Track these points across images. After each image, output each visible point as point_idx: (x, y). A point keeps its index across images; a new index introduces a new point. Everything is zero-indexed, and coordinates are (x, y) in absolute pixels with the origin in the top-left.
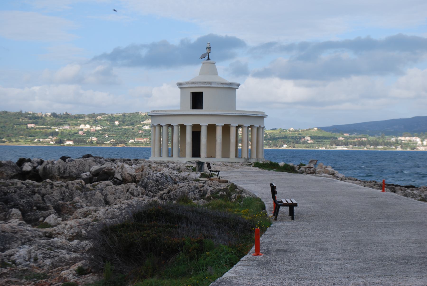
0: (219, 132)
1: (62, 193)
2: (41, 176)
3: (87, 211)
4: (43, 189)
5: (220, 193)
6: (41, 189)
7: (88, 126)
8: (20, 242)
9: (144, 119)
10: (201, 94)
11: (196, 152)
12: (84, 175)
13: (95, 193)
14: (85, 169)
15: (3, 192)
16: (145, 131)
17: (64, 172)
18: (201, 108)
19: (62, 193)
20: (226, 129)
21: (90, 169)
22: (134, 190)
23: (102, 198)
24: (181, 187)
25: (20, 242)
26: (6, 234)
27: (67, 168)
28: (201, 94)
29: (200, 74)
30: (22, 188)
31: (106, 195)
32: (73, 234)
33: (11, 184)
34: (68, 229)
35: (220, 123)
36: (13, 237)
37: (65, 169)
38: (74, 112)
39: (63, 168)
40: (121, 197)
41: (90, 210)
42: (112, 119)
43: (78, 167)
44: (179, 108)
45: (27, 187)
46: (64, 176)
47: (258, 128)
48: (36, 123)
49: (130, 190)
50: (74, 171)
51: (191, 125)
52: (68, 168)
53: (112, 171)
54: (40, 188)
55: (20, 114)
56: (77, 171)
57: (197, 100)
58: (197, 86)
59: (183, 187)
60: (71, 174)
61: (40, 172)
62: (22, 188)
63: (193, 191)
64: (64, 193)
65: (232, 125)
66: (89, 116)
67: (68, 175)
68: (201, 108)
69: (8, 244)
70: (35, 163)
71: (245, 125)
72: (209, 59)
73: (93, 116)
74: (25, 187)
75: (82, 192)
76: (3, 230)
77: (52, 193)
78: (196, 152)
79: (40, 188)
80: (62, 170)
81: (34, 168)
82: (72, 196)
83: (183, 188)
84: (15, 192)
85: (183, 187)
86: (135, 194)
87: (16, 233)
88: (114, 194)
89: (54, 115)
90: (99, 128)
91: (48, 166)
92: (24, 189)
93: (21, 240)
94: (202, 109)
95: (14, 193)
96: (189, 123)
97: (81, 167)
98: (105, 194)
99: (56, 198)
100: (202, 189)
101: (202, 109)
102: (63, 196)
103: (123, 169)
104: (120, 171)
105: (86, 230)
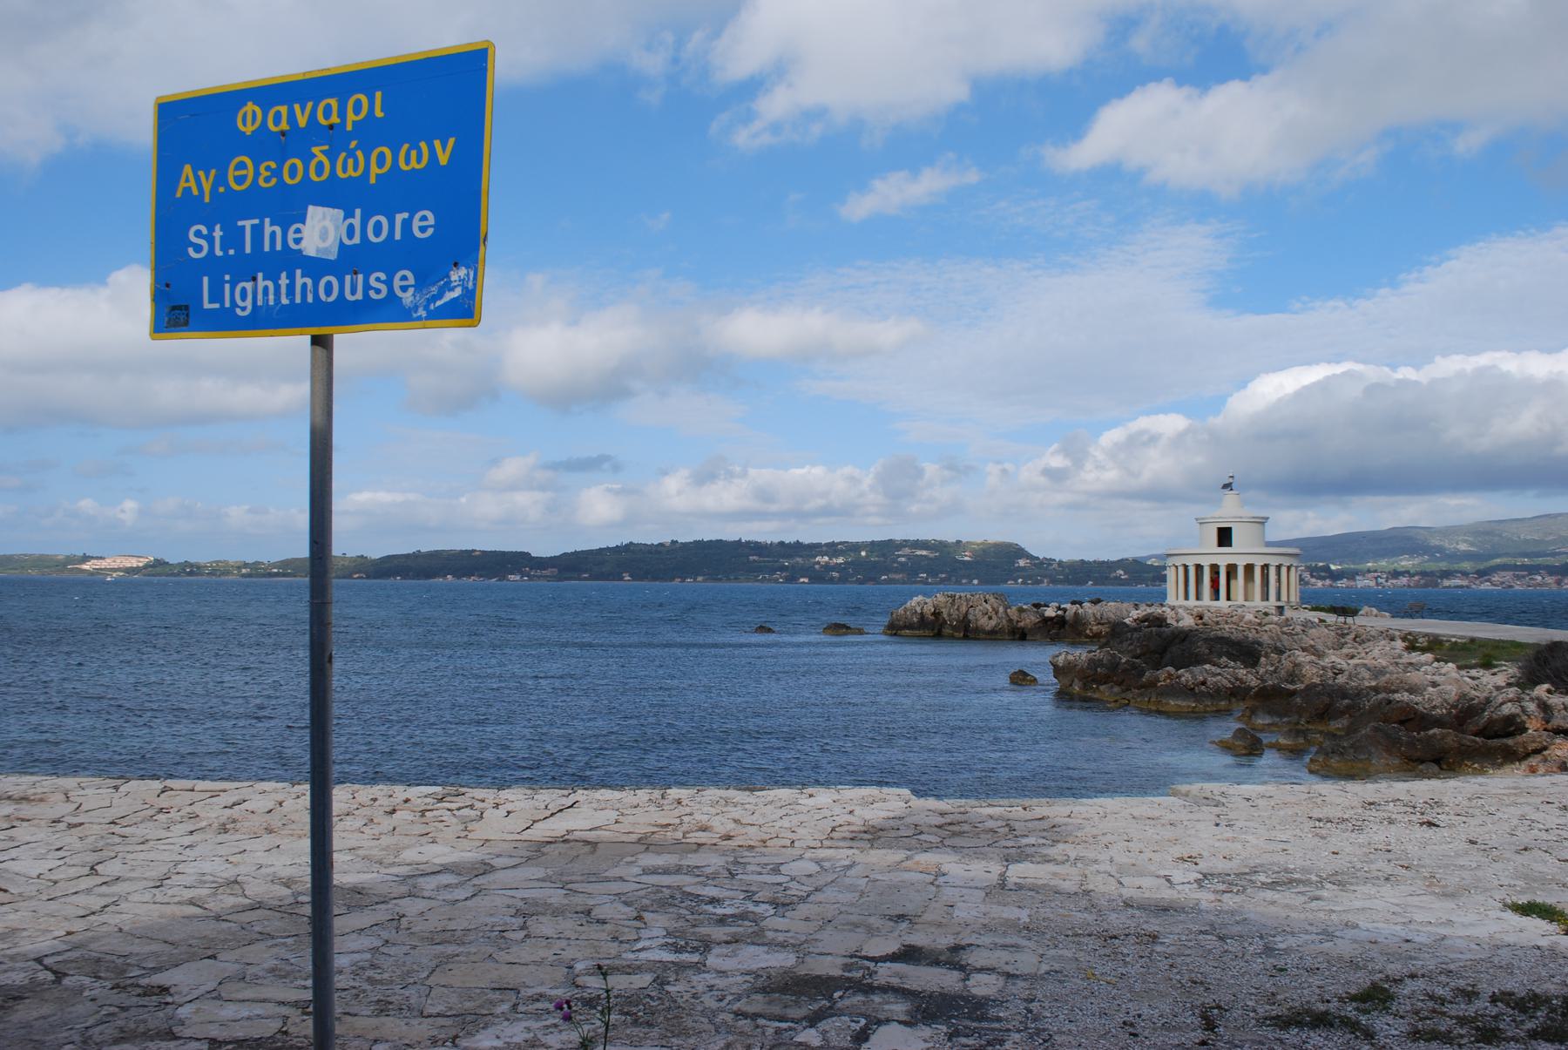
16: (901, 564)
57: (1224, 536)
90: (840, 560)
96: (1223, 563)
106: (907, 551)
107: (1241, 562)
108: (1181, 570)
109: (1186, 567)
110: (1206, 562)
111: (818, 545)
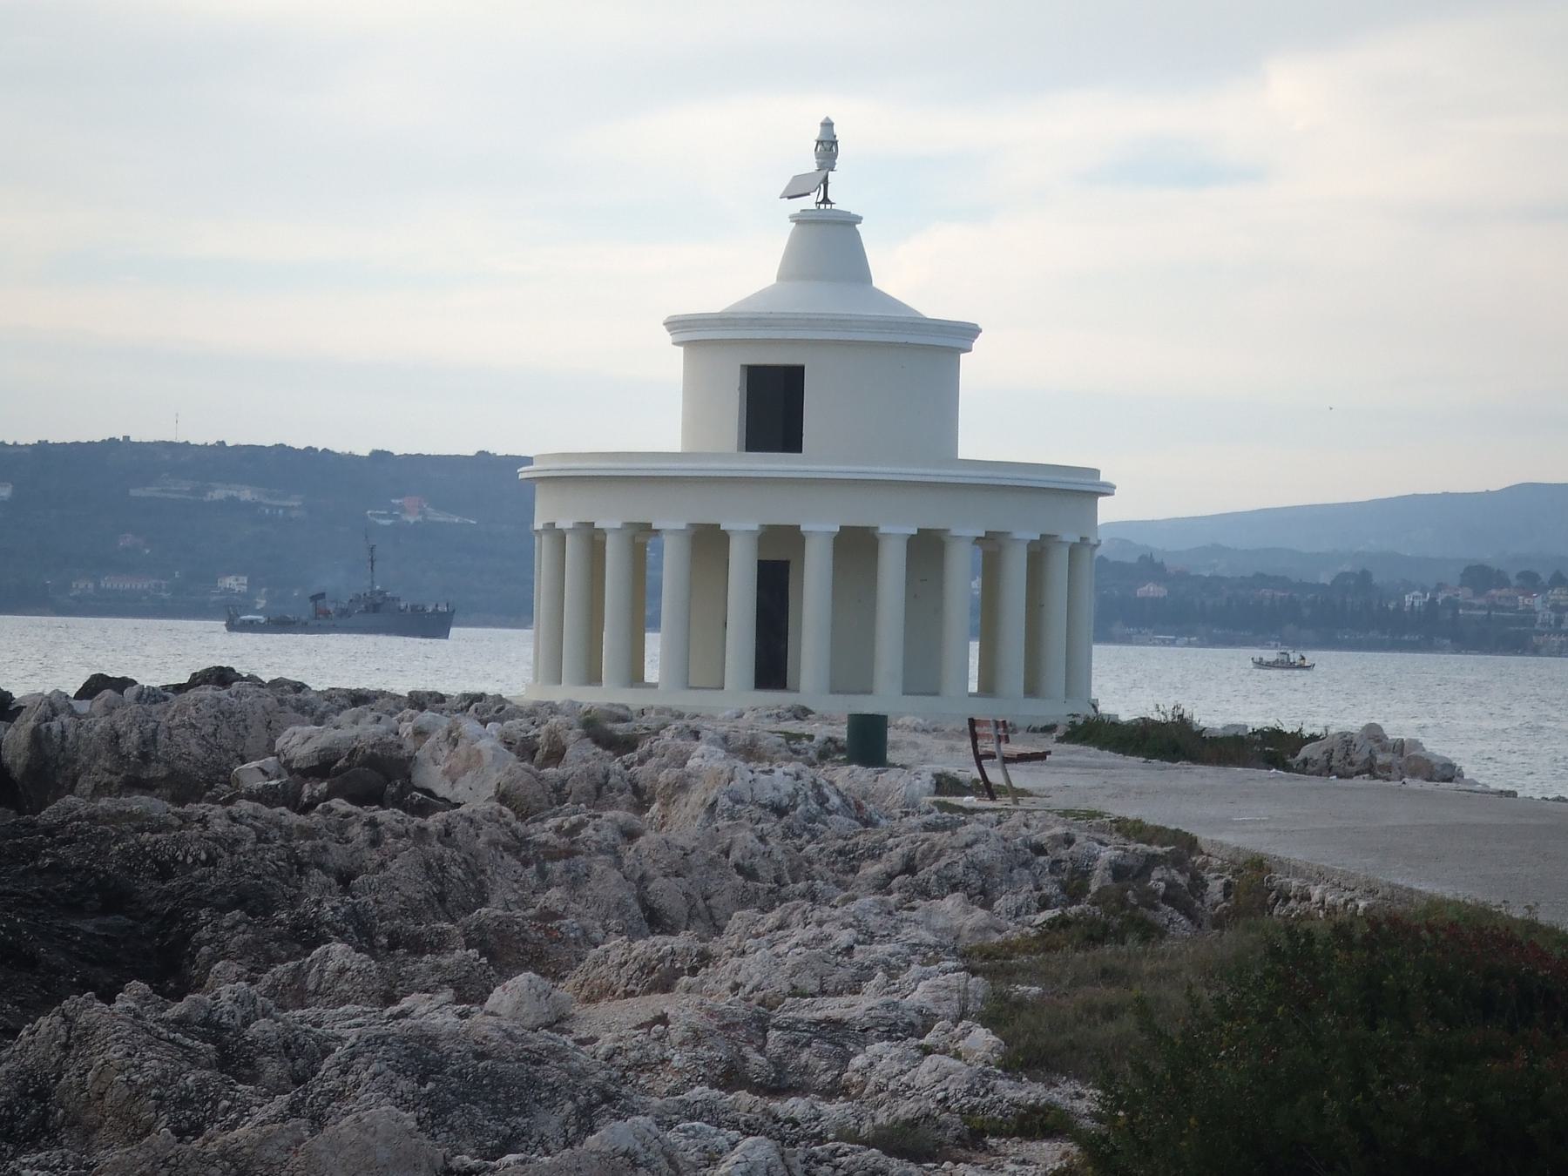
1: (429, 867)
2: (17, 773)
3: (661, 960)
4: (332, 846)
5: (1156, 874)
6: (325, 849)
8: (569, 1106)
10: (794, 375)
11: (772, 668)
12: (251, 774)
13: (589, 868)
14: (249, 741)
15: (155, 861)
17: (145, 757)
19: (429, 867)
20: (927, 549)
21: (272, 742)
22: (753, 855)
23: (627, 893)
24: (968, 846)
25: (569, 1106)
26: (501, 1067)
27: (155, 732)
28: (794, 375)
29: (779, 278)
30: (237, 842)
31: (643, 878)
32: (712, 1068)
33: (177, 822)
34: (682, 1044)
35: (896, 528)
36: (533, 1083)
37: (149, 741)
39: (134, 736)
40: (712, 887)
41: (673, 952)
43: (211, 729)
44: (676, 446)
45: (262, 838)
47: (1074, 550)
49: (735, 855)
50: (196, 750)
51: (755, 527)
52: (162, 737)
53: (404, 753)
54: (319, 842)
56: (210, 750)
57: (773, 406)
58: (791, 335)
59: (975, 842)
60: (181, 764)
62: (237, 842)
63: (1026, 864)
64: (442, 869)
65: (955, 532)
69: (517, 1114)
71: (1017, 535)
72: (826, 200)
74: (253, 835)
75: (526, 863)
76: (479, 1048)
77: (382, 865)
78: (772, 668)
79: (319, 842)
80: (131, 742)
82: (481, 883)
83: (975, 848)
84: (211, 861)
85: (975, 842)
86: (761, 873)
87: (538, 1062)
88: (677, 875)
91: (55, 726)
92: (248, 846)
93: (573, 1098)
94: (800, 451)
95: (204, 864)
98: (637, 876)
99: (409, 890)
100: (1063, 853)
101: (800, 451)
102: (442, 884)
105: (761, 1050)
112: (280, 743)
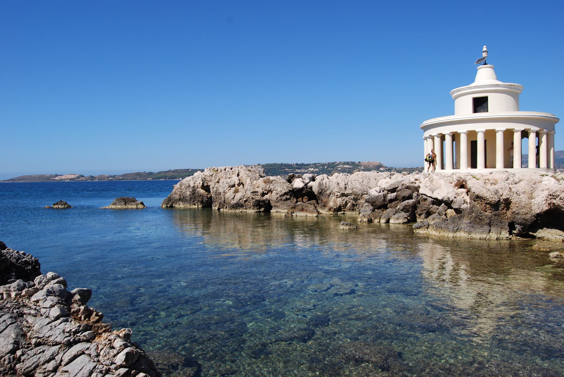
0: (500, 139)
2: (316, 193)
7: (313, 169)
9: (338, 165)
10: (485, 99)
17: (346, 188)
18: (486, 110)
38: (305, 163)
39: (343, 184)
42: (323, 165)
46: (346, 192)
48: (289, 168)
50: (358, 186)
52: (349, 183)
55: (282, 165)
60: (355, 190)
61: (313, 189)
66: (313, 164)
67: (351, 192)
68: (486, 110)
70: (307, 178)
73: (315, 164)
81: (306, 185)
89: (297, 164)
96: (481, 128)
97: (365, 181)
103: (432, 181)
104: (427, 185)
106: (341, 166)
107: (501, 127)
108: (437, 140)
109: (443, 138)
110: (462, 129)
111: (310, 165)
112: (379, 184)
